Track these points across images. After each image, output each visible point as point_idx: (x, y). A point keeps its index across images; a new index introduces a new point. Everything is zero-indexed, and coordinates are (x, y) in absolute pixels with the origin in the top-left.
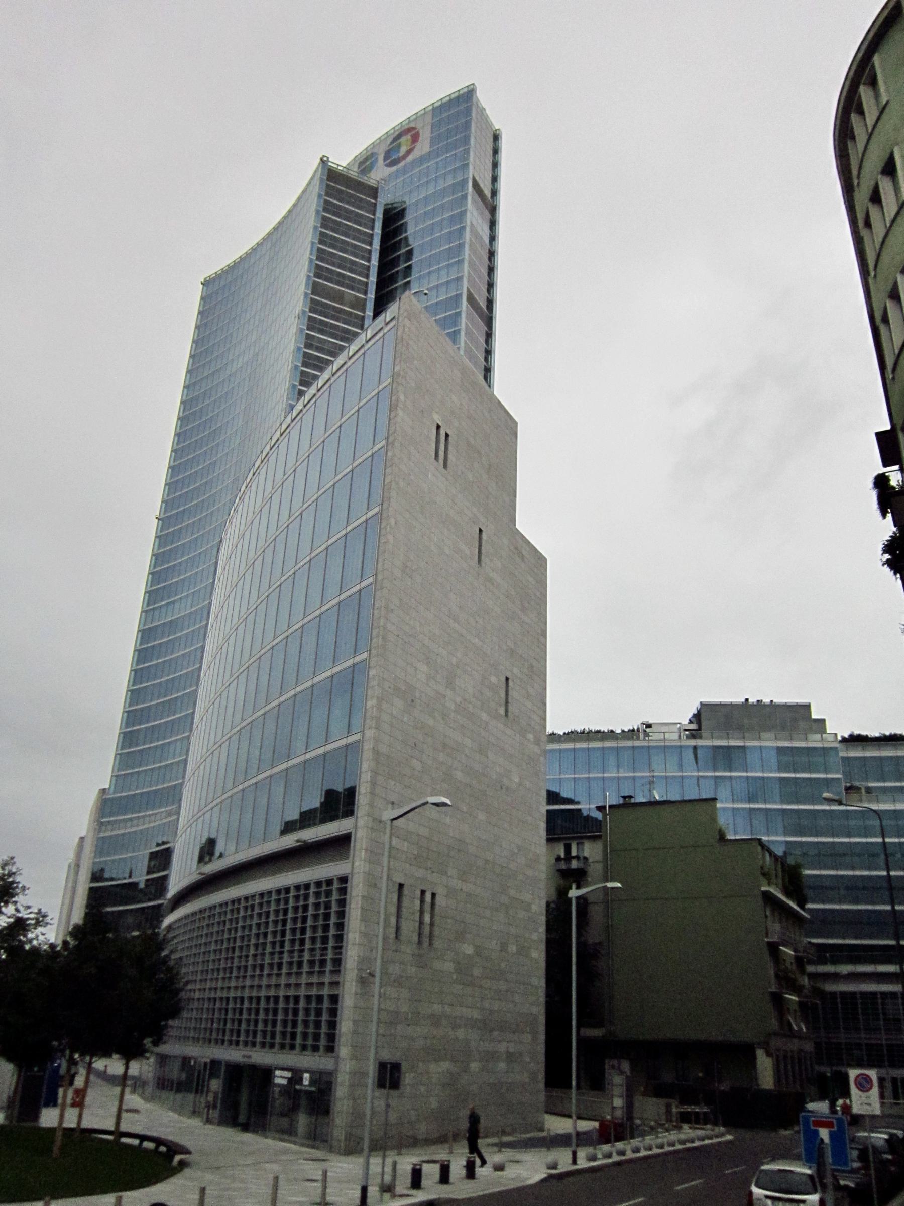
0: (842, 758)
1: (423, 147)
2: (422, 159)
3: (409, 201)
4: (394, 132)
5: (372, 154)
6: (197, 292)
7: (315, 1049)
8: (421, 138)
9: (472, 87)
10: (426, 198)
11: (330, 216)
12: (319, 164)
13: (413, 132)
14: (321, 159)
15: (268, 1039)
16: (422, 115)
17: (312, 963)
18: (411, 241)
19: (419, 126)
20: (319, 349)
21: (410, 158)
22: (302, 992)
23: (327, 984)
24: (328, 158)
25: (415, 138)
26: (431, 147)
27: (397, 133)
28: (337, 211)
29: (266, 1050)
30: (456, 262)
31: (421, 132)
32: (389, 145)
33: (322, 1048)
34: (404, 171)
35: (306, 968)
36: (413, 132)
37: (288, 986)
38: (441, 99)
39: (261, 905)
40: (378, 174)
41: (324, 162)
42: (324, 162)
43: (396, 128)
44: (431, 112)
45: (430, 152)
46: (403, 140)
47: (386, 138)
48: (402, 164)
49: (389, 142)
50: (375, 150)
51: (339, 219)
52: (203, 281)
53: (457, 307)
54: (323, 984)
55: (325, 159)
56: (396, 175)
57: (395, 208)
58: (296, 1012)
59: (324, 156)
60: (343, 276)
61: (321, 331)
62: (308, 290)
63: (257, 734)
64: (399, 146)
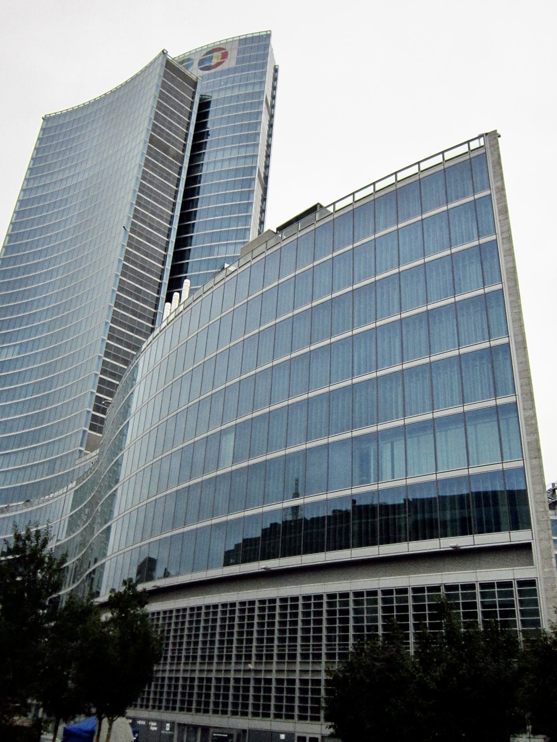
0: (551, 520)
1: (231, 63)
2: (229, 71)
3: (215, 97)
4: (208, 48)
5: (189, 60)
6: (40, 123)
7: (189, 710)
8: (229, 57)
9: (269, 32)
10: (238, 96)
11: (179, 91)
12: (160, 54)
13: (224, 51)
14: (163, 51)
15: (145, 703)
16: (231, 42)
17: (203, 657)
18: (209, 125)
19: (228, 48)
20: (150, 182)
21: (219, 68)
22: (181, 675)
23: (214, 671)
24: (167, 52)
25: (225, 56)
26: (236, 64)
27: (209, 49)
28: (170, 90)
29: (143, 709)
30: (252, 144)
31: (229, 53)
32: (204, 55)
33: (193, 710)
34: (215, 75)
35: (199, 660)
36: (224, 51)
37: (171, 671)
38: (240, 36)
39: (177, 617)
40: (195, 72)
41: (164, 53)
42: (164, 53)
43: (209, 46)
44: (238, 42)
45: (235, 68)
46: (215, 54)
47: (201, 50)
48: (213, 71)
49: (202, 54)
50: (192, 57)
51: (170, 95)
52: (44, 116)
53: (251, 175)
54: (211, 671)
55: (165, 52)
56: (208, 77)
57: (206, 99)
58: (176, 687)
59: (164, 50)
60: (170, 135)
61: (152, 170)
62: (147, 138)
63: (156, 472)
64: (211, 58)
